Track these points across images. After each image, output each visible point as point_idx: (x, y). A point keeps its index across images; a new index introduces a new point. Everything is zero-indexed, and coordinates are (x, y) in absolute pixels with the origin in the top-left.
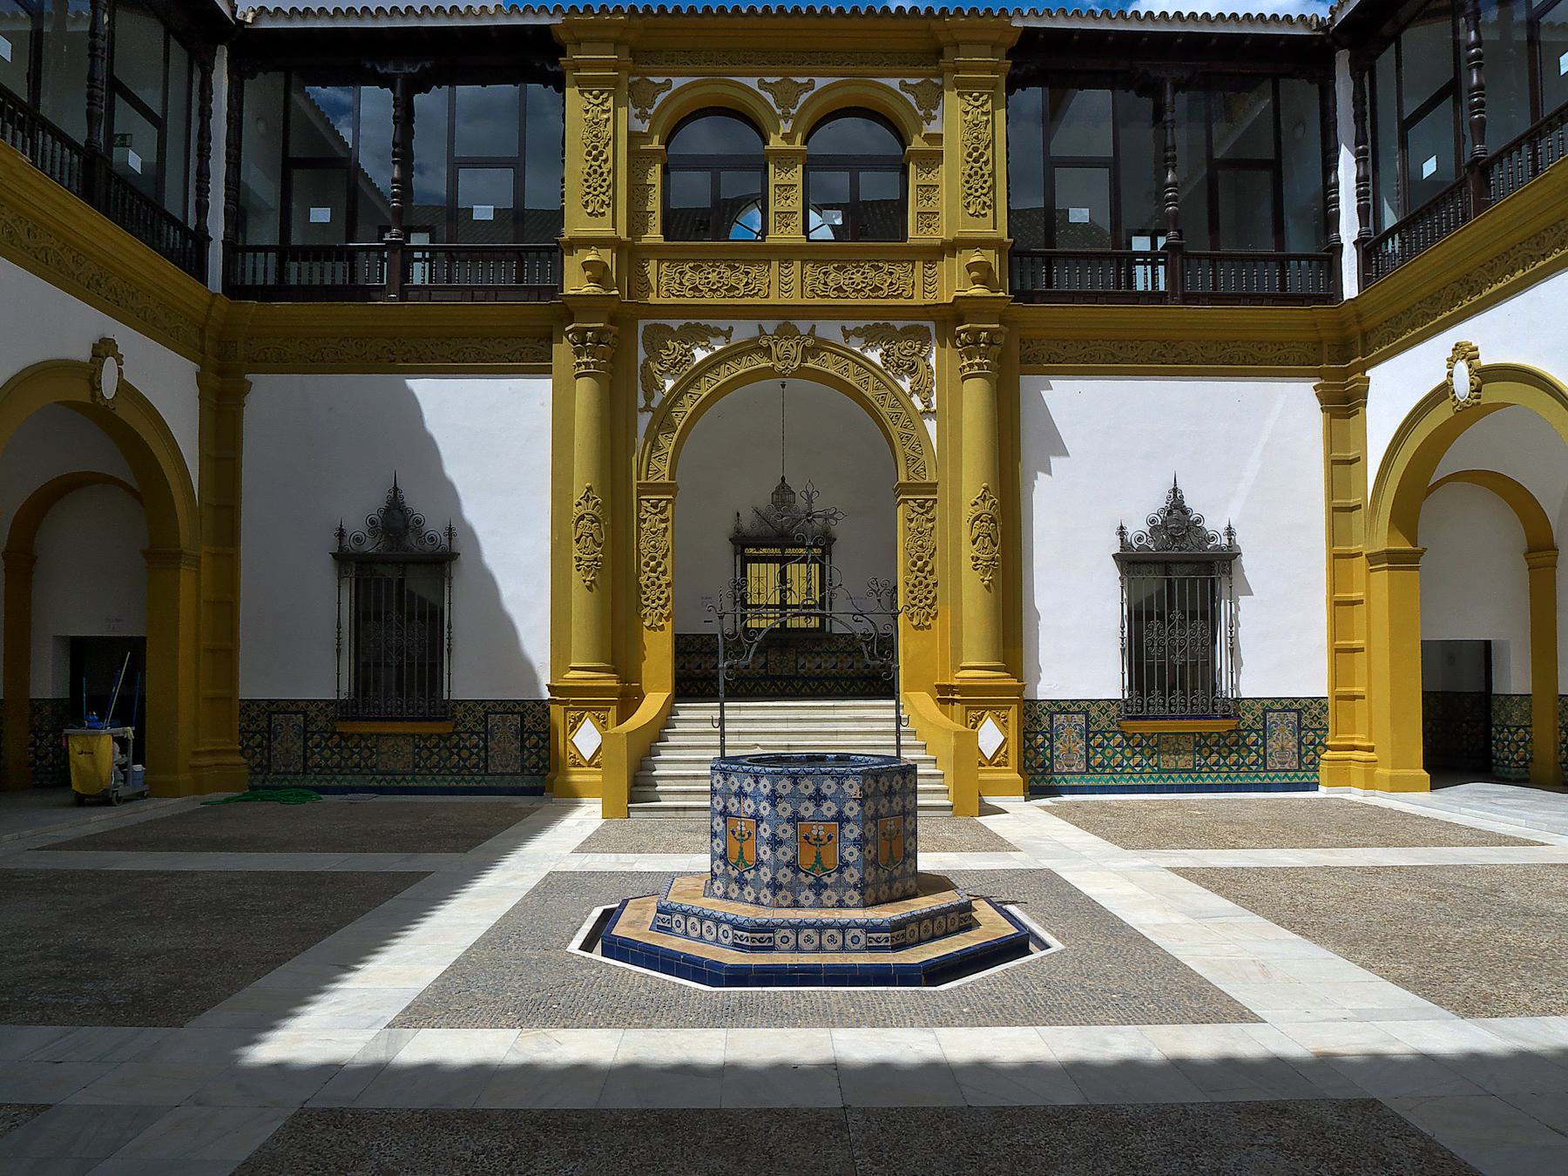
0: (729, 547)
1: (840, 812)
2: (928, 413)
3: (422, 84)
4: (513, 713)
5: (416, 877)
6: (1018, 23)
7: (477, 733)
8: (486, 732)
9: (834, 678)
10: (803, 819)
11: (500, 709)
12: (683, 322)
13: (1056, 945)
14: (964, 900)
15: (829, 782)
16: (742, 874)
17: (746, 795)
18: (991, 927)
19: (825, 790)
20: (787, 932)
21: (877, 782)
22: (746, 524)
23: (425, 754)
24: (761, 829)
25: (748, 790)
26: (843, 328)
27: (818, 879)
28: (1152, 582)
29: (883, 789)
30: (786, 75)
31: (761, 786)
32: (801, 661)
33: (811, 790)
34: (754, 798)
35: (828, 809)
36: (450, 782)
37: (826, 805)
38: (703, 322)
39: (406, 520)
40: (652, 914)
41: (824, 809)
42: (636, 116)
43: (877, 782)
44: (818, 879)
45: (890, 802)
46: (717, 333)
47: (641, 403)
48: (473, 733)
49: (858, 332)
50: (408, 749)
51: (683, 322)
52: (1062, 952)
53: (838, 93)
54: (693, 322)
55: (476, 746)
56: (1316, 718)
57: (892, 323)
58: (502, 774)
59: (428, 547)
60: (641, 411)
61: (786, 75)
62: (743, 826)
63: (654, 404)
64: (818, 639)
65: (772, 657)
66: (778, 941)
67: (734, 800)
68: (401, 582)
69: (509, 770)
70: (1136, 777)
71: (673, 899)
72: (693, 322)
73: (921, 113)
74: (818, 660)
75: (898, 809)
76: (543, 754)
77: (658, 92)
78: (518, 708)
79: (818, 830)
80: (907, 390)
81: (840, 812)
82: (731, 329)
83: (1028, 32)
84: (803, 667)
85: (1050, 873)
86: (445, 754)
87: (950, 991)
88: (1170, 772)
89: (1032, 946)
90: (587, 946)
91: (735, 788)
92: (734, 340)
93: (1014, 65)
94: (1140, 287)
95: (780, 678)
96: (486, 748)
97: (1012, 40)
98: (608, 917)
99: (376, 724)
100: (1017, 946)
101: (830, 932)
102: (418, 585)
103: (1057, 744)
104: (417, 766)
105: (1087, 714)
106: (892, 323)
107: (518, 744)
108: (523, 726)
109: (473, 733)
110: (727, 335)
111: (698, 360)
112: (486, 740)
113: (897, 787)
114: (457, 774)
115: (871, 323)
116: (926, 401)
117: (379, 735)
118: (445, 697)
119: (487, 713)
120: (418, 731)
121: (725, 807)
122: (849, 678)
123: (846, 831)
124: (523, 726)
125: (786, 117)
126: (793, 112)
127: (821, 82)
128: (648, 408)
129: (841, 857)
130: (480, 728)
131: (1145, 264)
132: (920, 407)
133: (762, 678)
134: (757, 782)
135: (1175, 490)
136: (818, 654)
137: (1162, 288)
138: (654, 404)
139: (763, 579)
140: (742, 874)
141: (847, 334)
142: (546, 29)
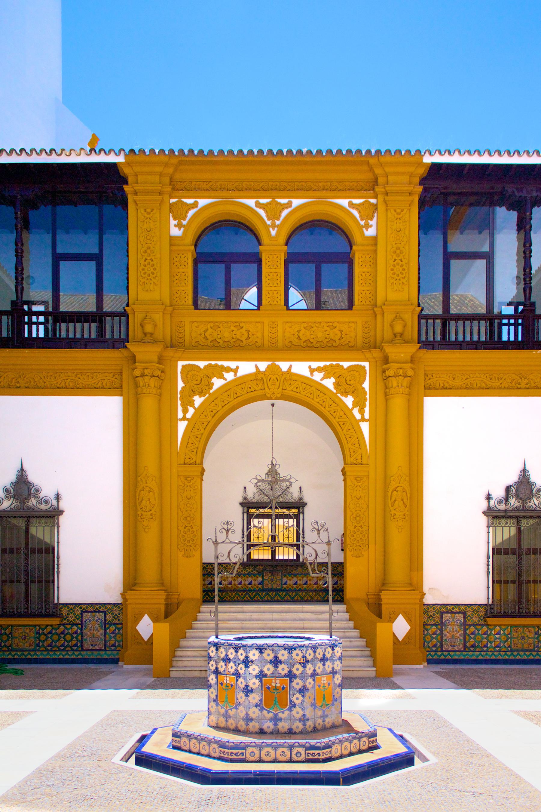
0: (240, 509)
1: (290, 672)
2: (363, 419)
3: (32, 204)
4: (99, 612)
5: (24, 714)
6: (428, 160)
7: (76, 625)
8: (82, 624)
9: (305, 590)
10: (266, 676)
11: (91, 609)
12: (206, 363)
13: (433, 759)
14: (372, 730)
15: (283, 651)
16: (227, 712)
17: (229, 660)
18: (390, 747)
19: (280, 657)
20: (254, 749)
21: (315, 652)
22: (252, 494)
23: (43, 638)
24: (239, 682)
25: (231, 656)
26: (310, 367)
27: (276, 715)
28: (507, 532)
29: (320, 656)
30: (273, 198)
31: (239, 654)
32: (285, 580)
33: (272, 657)
34: (235, 662)
35: (283, 669)
36: (59, 655)
37: (281, 667)
38: (220, 363)
39: (29, 490)
40: (170, 738)
41: (280, 669)
42: (175, 226)
43: (315, 652)
44: (276, 715)
45: (324, 665)
46: (228, 370)
47: (180, 415)
48: (74, 624)
49: (319, 369)
50: (32, 635)
51: (206, 363)
52: (435, 764)
53: (306, 211)
54: (213, 363)
55: (76, 633)
56: (116, 617)
57: (341, 363)
58: (92, 650)
59: (44, 507)
60: (181, 420)
61: (273, 198)
62: (227, 680)
63: (189, 416)
64: (296, 566)
65: (266, 577)
66: (248, 755)
67: (222, 663)
68: (27, 530)
69: (97, 648)
70: (496, 654)
71: (183, 728)
72: (213, 363)
73: (362, 223)
74: (295, 579)
75: (329, 670)
76: (118, 638)
77: (189, 209)
78: (103, 609)
79: (277, 683)
80: (350, 405)
81: (290, 672)
82: (238, 367)
83: (435, 168)
84: (286, 583)
85: (433, 712)
86: (55, 637)
87: (358, 788)
88: (518, 650)
89: (416, 760)
90: (126, 759)
91: (223, 656)
92: (240, 373)
93: (425, 190)
94: (505, 338)
95: (271, 590)
96: (82, 633)
97: (422, 171)
98: (143, 739)
99: (13, 619)
100: (406, 760)
101: (281, 749)
102: (38, 531)
103: (445, 633)
104: (37, 645)
105: (464, 613)
106: (341, 363)
107: (102, 631)
108: (105, 620)
109: (74, 624)
110: (236, 371)
111: (215, 387)
112: (82, 629)
113: (328, 656)
114: (63, 650)
115: (328, 363)
116: (362, 412)
117: (13, 626)
118: (56, 602)
119: (83, 612)
120: (50, 623)
121: (217, 668)
122: (315, 591)
123: (294, 684)
124: (105, 620)
125: (274, 226)
126: (278, 222)
127: (296, 202)
128: (184, 418)
129: (291, 701)
130: (78, 621)
131: (509, 324)
132: (358, 416)
133: (260, 590)
134: (236, 652)
135: (524, 470)
136: (295, 575)
137: (520, 339)
138: (189, 416)
139: (262, 527)
140: (227, 712)
141: (312, 371)
142: (113, 166)
